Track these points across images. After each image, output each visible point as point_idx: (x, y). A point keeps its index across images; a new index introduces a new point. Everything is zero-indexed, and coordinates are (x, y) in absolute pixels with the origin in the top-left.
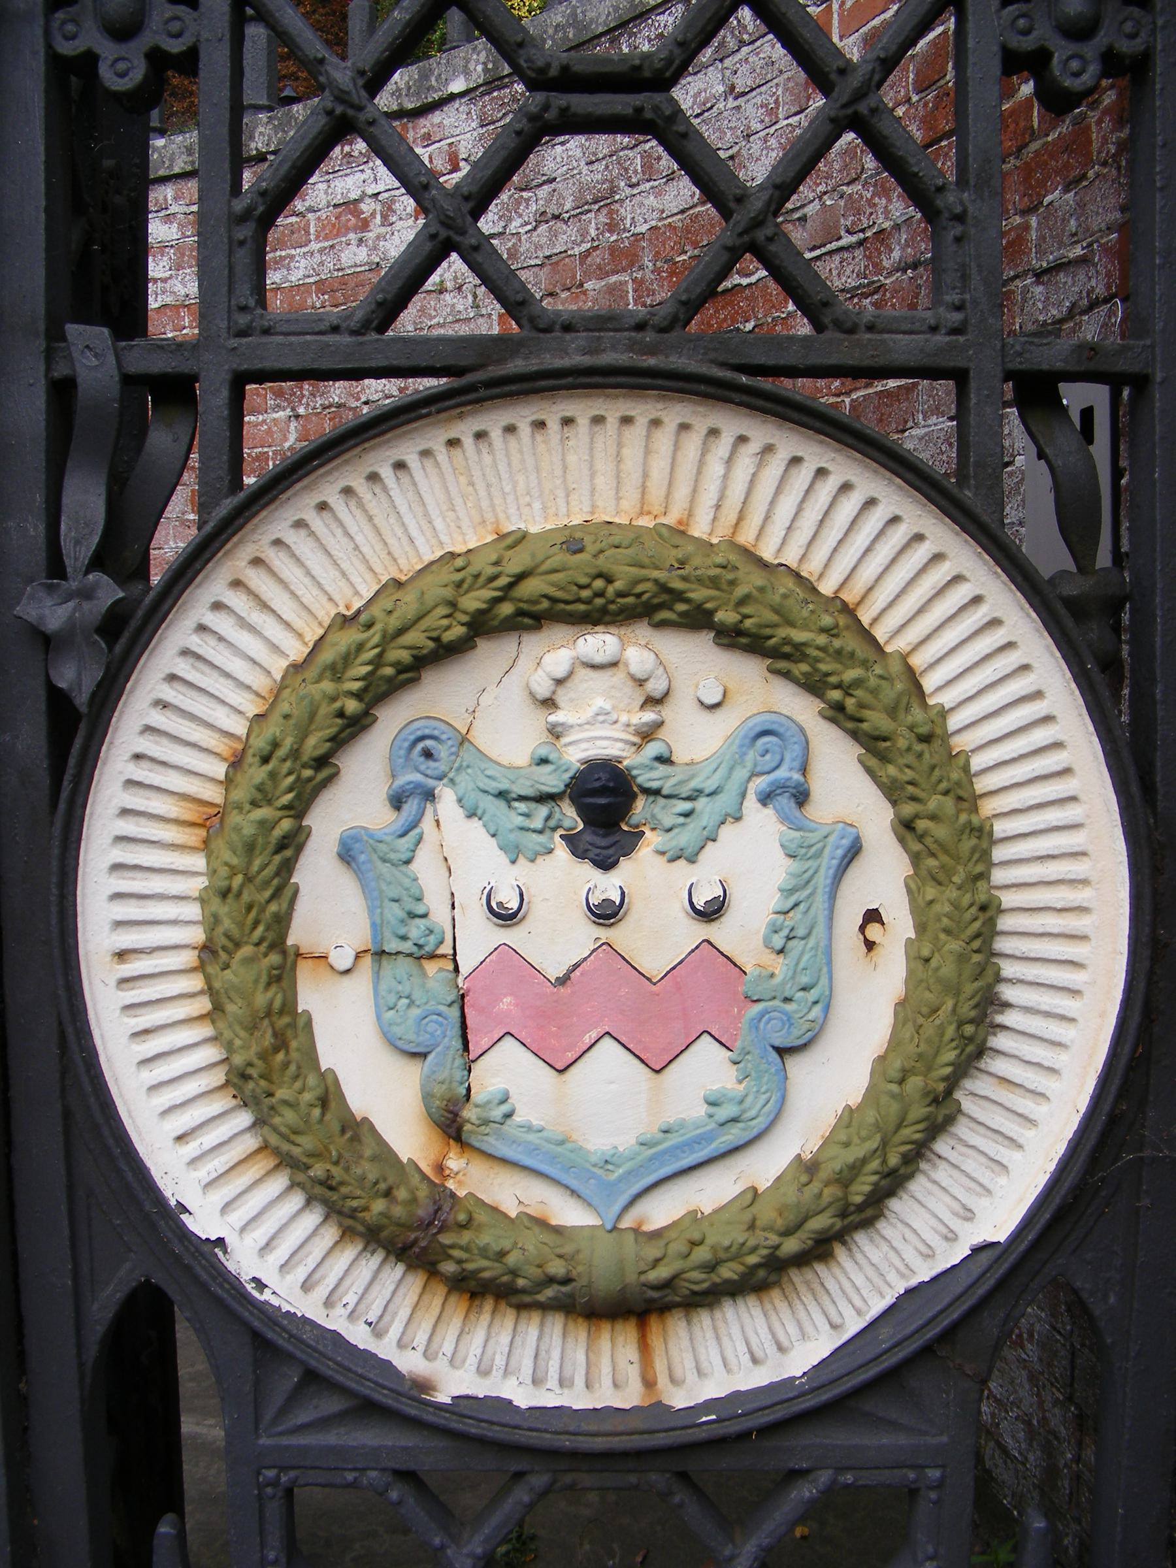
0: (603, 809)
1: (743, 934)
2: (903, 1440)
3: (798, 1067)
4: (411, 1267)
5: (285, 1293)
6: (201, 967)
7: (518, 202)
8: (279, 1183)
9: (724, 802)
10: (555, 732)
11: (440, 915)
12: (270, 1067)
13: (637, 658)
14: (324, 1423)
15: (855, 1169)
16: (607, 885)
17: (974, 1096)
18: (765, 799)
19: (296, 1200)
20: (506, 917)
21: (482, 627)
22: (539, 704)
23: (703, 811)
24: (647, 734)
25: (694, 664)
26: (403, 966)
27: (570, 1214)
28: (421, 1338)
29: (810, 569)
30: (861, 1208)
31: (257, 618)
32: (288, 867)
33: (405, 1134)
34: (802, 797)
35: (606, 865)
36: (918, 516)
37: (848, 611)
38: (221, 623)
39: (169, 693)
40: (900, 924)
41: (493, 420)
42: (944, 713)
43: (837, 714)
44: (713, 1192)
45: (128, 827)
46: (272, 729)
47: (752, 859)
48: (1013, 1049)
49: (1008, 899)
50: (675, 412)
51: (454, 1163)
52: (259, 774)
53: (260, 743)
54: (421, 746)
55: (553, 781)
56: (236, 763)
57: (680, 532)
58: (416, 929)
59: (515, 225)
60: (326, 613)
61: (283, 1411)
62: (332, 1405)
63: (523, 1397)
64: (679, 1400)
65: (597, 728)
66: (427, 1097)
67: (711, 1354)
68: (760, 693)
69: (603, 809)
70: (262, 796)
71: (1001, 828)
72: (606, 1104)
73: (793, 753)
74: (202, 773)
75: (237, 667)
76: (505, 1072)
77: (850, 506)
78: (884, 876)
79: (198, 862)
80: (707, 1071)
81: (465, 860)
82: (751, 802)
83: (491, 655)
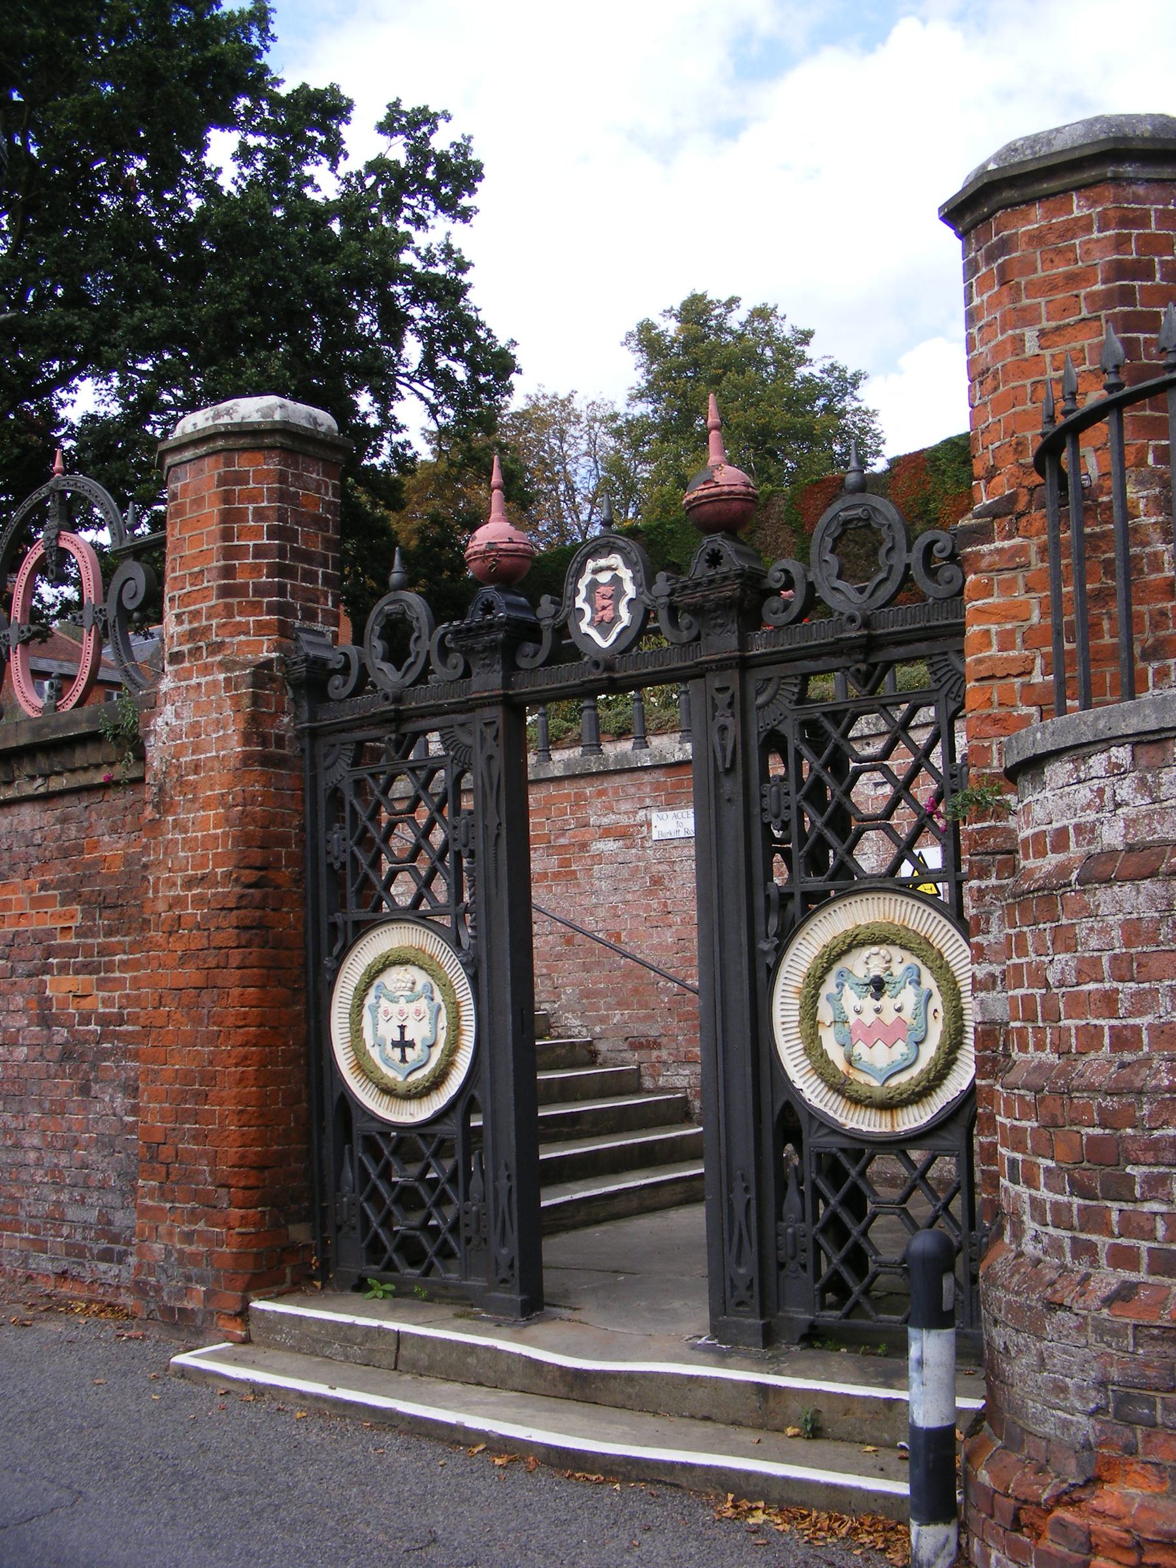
1: (907, 1015)
3: (921, 1047)
5: (815, 1103)
13: (883, 952)
16: (878, 1004)
20: (858, 1012)
22: (865, 963)
24: (887, 969)
25: (896, 953)
27: (875, 1083)
32: (815, 1002)
33: (841, 1065)
34: (919, 983)
40: (941, 1014)
41: (852, 900)
44: (903, 1078)
47: (908, 997)
54: (841, 974)
55: (867, 981)
62: (825, 1131)
63: (865, 1128)
68: (911, 960)
69: (878, 986)
76: (860, 1049)
78: (937, 1002)
80: (901, 1048)
81: (851, 999)
83: (855, 953)
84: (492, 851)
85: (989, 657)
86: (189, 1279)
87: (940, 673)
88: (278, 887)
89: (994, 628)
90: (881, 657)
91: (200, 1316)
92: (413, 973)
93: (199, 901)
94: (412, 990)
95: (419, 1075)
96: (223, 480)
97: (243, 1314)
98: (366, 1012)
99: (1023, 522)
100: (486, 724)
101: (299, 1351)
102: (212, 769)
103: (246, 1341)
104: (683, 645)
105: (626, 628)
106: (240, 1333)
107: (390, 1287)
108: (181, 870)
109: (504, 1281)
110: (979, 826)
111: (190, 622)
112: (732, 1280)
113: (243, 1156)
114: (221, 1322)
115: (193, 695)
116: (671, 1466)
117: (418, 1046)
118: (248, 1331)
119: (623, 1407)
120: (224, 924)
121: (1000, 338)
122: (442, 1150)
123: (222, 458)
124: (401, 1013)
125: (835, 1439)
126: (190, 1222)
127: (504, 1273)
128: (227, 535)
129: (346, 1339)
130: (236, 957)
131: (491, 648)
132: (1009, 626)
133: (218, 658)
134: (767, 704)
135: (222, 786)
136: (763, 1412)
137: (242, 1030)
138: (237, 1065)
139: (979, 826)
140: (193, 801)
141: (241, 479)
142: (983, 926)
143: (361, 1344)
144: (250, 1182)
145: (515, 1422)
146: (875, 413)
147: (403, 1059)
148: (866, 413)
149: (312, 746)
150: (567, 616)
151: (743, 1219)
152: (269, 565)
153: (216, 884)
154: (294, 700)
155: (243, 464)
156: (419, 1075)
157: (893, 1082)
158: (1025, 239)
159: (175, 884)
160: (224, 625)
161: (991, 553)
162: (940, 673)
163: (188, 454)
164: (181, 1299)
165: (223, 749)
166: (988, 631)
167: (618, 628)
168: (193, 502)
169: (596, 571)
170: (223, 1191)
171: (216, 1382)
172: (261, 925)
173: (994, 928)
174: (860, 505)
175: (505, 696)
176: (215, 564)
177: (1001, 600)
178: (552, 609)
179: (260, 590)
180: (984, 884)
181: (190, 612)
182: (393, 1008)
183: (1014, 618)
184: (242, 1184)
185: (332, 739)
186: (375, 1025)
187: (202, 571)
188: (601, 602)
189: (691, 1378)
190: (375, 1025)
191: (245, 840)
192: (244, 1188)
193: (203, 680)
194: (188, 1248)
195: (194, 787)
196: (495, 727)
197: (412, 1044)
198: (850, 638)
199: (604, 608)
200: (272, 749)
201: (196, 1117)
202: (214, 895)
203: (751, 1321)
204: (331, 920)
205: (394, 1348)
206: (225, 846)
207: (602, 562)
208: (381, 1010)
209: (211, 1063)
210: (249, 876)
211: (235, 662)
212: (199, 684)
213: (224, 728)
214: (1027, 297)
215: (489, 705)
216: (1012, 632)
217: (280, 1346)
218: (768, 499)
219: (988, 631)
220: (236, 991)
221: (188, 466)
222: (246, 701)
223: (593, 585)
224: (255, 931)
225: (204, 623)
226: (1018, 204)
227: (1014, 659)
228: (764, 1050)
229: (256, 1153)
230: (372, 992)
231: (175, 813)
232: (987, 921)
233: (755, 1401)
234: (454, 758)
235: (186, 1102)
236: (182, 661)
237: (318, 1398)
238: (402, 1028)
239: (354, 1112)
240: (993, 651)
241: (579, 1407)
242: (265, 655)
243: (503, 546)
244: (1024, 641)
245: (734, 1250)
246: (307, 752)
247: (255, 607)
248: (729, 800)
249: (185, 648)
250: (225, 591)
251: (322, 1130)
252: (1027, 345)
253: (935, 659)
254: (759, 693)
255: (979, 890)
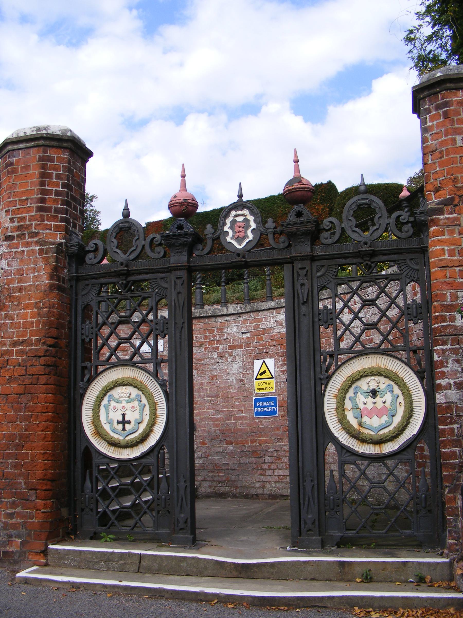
0: (374, 393)
1: (388, 405)
2: (407, 457)
4: (357, 440)
6: (336, 410)
7: (368, 311)
8: (344, 431)
9: (385, 392)
10: (369, 386)
11: (359, 404)
12: (343, 420)
14: (348, 456)
15: (400, 427)
16: (374, 400)
17: (412, 420)
18: (389, 392)
19: (345, 433)
20: (365, 404)
21: (362, 377)
22: (367, 384)
23: (383, 393)
24: (378, 386)
25: (382, 379)
26: (355, 409)
27: (372, 433)
28: (358, 447)
29: (392, 370)
30: (400, 431)
31: (341, 377)
32: (344, 400)
33: (356, 426)
34: (393, 392)
35: (374, 399)
36: (405, 366)
37: (396, 374)
38: (337, 377)
39: (332, 384)
40: (403, 403)
42: (406, 383)
43: (395, 383)
44: (386, 431)
45: (329, 397)
46: (343, 387)
47: (388, 397)
48: (415, 416)
49: (413, 401)
50: (379, 356)
51: (361, 429)
52: (341, 391)
53: (341, 388)
55: (369, 391)
56: (339, 390)
57: (380, 367)
58: (356, 406)
59: (367, 316)
60: (347, 376)
61: (344, 455)
64: (384, 452)
65: (373, 386)
66: (358, 422)
67: (387, 448)
69: (374, 393)
70: (342, 393)
71: (412, 394)
72: (375, 422)
73: (391, 387)
74: (336, 392)
75: (339, 381)
76: (366, 419)
77: (396, 364)
78: (401, 399)
79: (336, 400)
80: (385, 418)
81: (361, 399)
82: (388, 392)
84: (178, 334)
85: (445, 259)
86: (10, 536)
87: (402, 267)
88: (61, 348)
89: (446, 248)
90: (377, 259)
91: (18, 555)
92: (130, 389)
93: (20, 353)
94: (129, 397)
95: (132, 436)
96: (41, 159)
97: (45, 552)
98: (102, 408)
99: (457, 208)
100: (177, 278)
101: (79, 567)
102: (30, 291)
103: (46, 565)
104: (280, 249)
105: (251, 241)
106: (43, 561)
107: (111, 536)
108: (9, 338)
109: (181, 529)
110: (442, 324)
111: (18, 222)
112: (305, 521)
113: (45, 475)
114: (30, 557)
115: (19, 256)
116: (322, 599)
117: (133, 423)
118: (47, 560)
119: (269, 579)
120: (37, 363)
121: (444, 138)
122: (145, 470)
123: (42, 149)
124: (123, 408)
125: (378, 582)
126: (11, 508)
127: (181, 525)
128: (42, 184)
129: (109, 560)
130: (43, 379)
131: (183, 245)
132: (452, 248)
133: (36, 239)
134: (321, 276)
135: (36, 298)
136: (343, 574)
137: (45, 414)
138: (42, 431)
139: (442, 324)
140: (17, 305)
141: (51, 159)
142: (444, 364)
143: (118, 561)
144: (48, 487)
145: (226, 588)
146: (99, 212)
147: (124, 429)
148: (95, 212)
149: (76, 285)
150: (220, 234)
151: (310, 493)
152: (62, 200)
153: (32, 345)
154: (69, 263)
155: (51, 153)
156: (132, 436)
157: (381, 433)
158: (456, 103)
159: (5, 344)
160: (40, 224)
161: (444, 219)
162: (402, 267)
163: (22, 146)
164: (5, 547)
165: (37, 281)
166: (444, 249)
167: (247, 241)
168: (22, 168)
169: (236, 216)
170: (33, 492)
171: (48, 584)
172: (55, 366)
173: (450, 365)
174: (366, 199)
175: (189, 266)
176: (35, 196)
177: (449, 237)
178: (212, 231)
179: (57, 210)
180: (445, 348)
181: (19, 218)
182: (119, 406)
183: (455, 244)
184: (44, 488)
185: (87, 282)
186: (107, 414)
187: (27, 199)
188: (237, 229)
189: (305, 562)
190: (107, 414)
191: (50, 324)
192: (45, 490)
193: (25, 249)
194: (10, 521)
195: (19, 299)
196: (182, 280)
197: (129, 422)
198: (365, 251)
199: (240, 232)
200: (61, 284)
201: (15, 456)
202: (29, 350)
203: (314, 538)
204: (84, 365)
205: (138, 562)
206: (37, 326)
207: (240, 212)
208: (111, 407)
209: (26, 430)
210: (50, 341)
211: (45, 242)
212: (23, 251)
213: (38, 271)
214: (457, 124)
215: (180, 270)
216: (454, 250)
217: (66, 566)
218: (93, 234)
219: (444, 249)
220: (43, 395)
221: (20, 151)
222: (53, 260)
223: (234, 222)
224: (52, 368)
225: (27, 223)
226: (453, 89)
227: (455, 260)
228: (320, 420)
229: (51, 473)
230: (106, 399)
231: (6, 311)
232: (447, 362)
233: (338, 569)
234: (157, 293)
235: (9, 449)
236: (13, 240)
237: (114, 586)
238: (124, 415)
239: (93, 455)
240: (446, 256)
241: (247, 580)
242: (58, 240)
243: (190, 201)
244: (459, 253)
245: (316, 504)
246: (74, 287)
247: (54, 218)
248: (304, 315)
249: (15, 234)
250: (40, 209)
251: (75, 463)
252: (458, 142)
253: (400, 262)
254: (318, 271)
255: (443, 350)
